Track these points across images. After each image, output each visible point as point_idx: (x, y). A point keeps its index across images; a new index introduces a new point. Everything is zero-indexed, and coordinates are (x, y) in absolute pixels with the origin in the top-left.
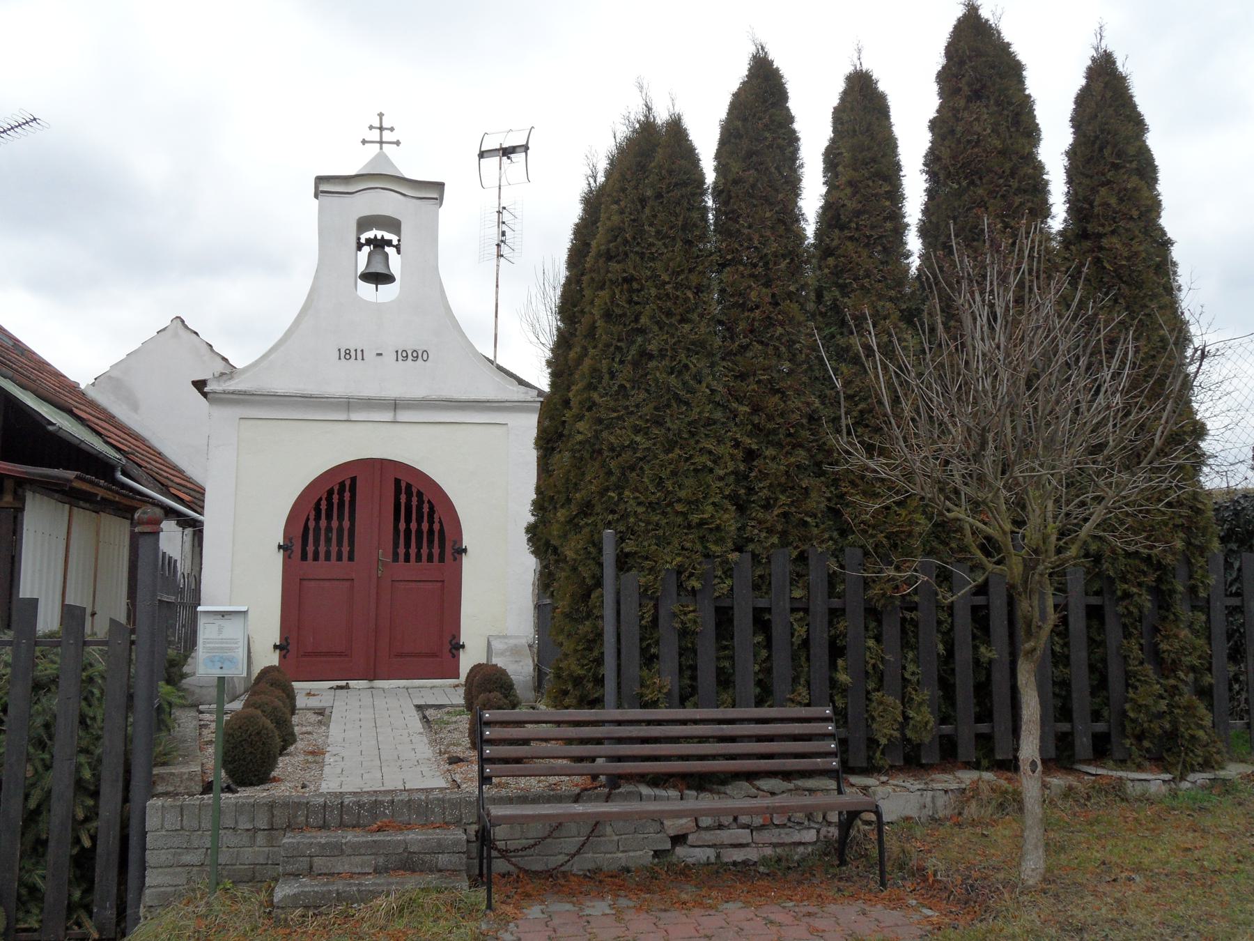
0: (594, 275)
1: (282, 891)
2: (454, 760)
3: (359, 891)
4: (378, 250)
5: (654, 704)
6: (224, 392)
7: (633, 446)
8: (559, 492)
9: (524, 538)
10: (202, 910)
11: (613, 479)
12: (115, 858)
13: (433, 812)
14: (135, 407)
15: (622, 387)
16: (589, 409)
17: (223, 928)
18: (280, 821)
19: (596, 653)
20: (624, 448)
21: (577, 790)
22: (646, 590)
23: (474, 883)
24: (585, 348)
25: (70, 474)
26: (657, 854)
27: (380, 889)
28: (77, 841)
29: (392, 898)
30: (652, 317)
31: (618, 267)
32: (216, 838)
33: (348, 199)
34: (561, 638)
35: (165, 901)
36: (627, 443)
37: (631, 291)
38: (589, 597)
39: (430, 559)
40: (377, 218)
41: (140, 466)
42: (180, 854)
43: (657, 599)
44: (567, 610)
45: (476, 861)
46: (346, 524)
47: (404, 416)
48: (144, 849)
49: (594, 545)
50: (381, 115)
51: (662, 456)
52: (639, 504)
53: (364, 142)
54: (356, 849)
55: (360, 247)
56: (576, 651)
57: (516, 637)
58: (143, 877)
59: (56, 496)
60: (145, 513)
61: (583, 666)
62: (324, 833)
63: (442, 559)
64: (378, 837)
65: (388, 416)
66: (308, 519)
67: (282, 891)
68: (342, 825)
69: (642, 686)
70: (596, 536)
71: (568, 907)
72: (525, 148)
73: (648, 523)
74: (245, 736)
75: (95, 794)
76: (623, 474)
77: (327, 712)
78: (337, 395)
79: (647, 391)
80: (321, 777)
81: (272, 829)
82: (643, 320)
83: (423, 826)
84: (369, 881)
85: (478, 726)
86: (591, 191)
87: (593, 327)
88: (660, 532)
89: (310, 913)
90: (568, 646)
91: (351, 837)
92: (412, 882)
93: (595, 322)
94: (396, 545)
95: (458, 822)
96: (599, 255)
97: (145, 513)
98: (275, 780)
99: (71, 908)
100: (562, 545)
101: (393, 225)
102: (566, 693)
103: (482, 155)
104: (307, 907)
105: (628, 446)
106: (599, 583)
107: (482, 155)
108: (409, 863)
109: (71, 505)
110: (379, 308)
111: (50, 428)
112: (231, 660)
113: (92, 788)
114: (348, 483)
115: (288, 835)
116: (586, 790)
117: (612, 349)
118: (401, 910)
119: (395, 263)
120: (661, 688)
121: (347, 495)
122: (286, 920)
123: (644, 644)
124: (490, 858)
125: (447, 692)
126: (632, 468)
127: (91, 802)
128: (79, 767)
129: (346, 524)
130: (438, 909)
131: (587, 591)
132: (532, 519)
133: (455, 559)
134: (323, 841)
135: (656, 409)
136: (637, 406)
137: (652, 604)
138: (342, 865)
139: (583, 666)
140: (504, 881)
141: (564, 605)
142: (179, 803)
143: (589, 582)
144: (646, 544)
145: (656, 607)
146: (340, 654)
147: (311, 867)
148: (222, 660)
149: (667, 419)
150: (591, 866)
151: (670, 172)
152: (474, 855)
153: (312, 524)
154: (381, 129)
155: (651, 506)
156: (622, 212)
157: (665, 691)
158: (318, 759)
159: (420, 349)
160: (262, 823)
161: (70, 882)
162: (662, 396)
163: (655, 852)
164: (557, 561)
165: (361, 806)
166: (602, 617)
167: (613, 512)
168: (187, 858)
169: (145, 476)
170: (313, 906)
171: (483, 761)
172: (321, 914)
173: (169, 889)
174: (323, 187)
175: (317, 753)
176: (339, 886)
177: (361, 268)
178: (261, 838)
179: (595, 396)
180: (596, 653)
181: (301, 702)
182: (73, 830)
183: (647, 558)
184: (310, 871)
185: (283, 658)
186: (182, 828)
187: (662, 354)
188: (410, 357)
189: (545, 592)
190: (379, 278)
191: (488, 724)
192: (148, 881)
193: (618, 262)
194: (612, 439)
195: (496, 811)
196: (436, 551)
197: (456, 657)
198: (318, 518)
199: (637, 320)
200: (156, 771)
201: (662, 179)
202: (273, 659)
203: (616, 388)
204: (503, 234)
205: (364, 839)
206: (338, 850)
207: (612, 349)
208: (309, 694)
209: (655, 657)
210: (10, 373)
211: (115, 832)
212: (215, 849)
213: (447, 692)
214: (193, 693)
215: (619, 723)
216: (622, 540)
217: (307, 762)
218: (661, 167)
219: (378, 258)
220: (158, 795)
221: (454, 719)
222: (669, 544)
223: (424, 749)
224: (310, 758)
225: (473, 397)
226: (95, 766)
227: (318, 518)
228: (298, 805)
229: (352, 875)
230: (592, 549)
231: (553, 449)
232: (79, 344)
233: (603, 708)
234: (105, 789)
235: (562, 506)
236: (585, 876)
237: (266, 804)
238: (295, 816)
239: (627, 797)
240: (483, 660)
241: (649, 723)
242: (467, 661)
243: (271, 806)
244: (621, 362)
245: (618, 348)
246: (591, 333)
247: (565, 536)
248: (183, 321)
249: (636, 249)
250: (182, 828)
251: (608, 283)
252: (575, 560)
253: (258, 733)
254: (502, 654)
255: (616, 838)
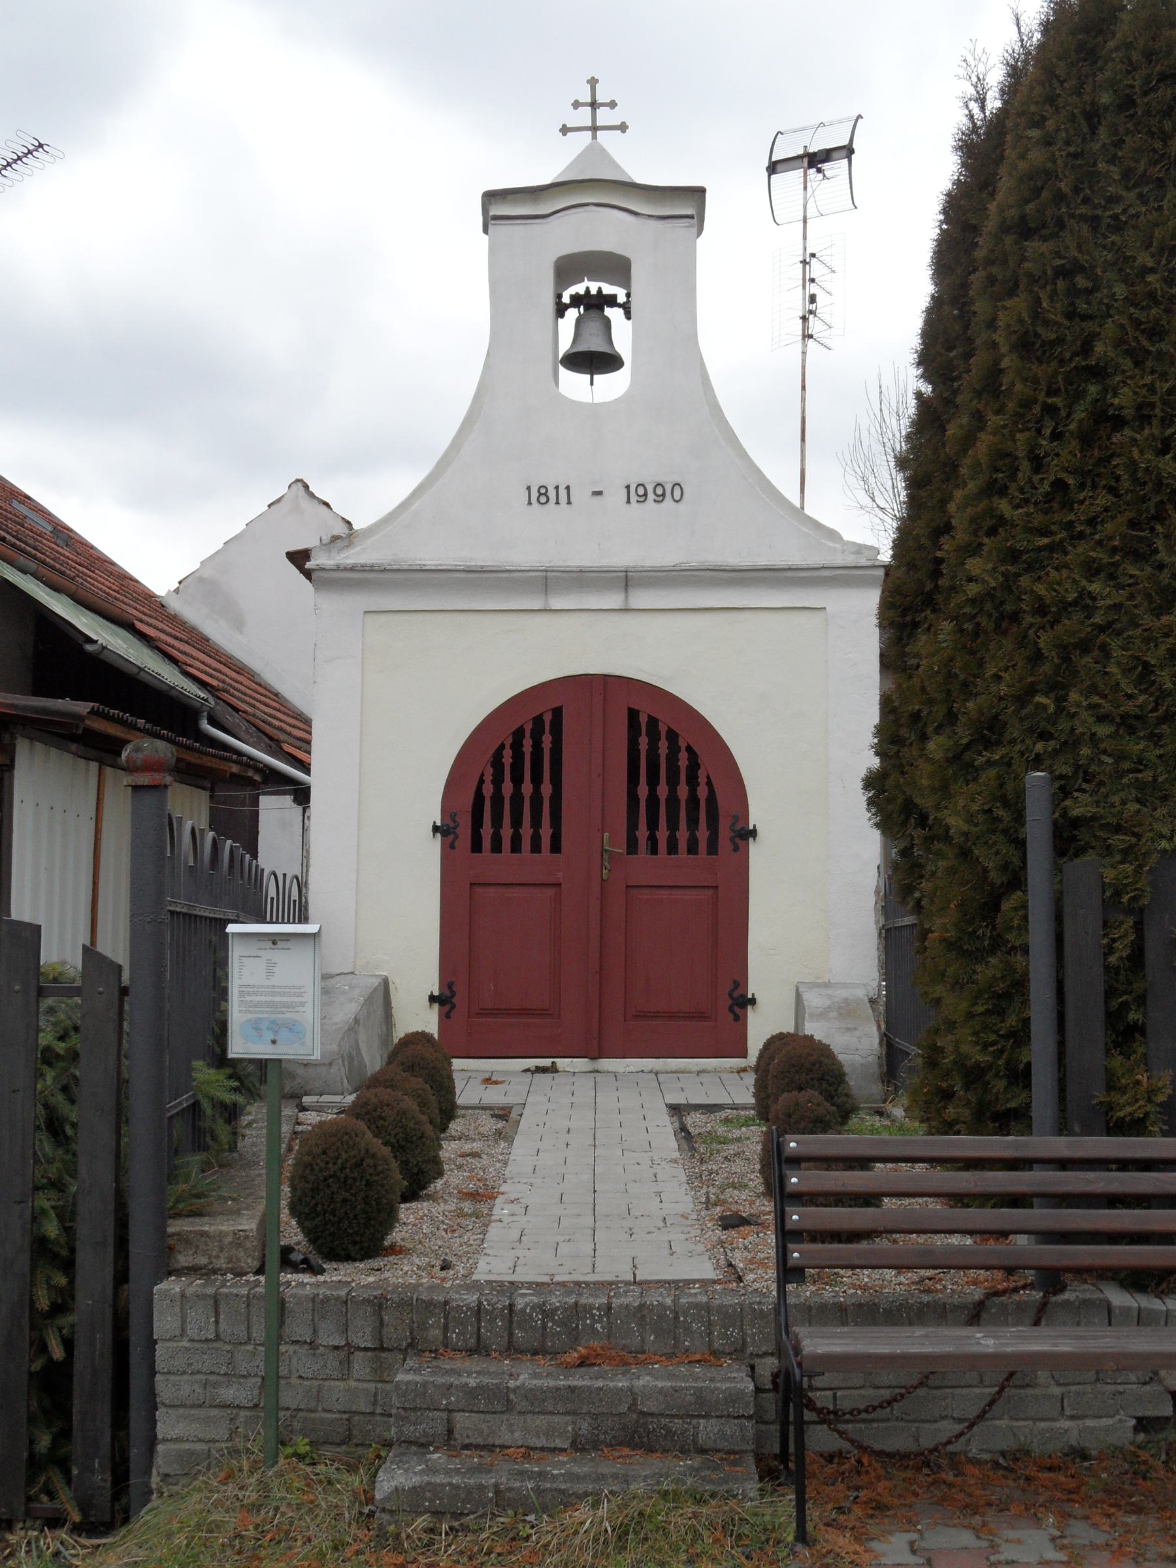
0: (994, 270)
1: (393, 1479)
2: (733, 1222)
3: (538, 1491)
4: (594, 313)
5: (1135, 1127)
6: (338, 569)
7: (1085, 603)
8: (931, 702)
9: (860, 798)
10: (251, 1495)
11: (1046, 668)
12: (105, 1384)
13: (688, 1329)
14: (239, 624)
15: (1059, 485)
16: (992, 532)
17: (285, 1536)
18: (396, 1332)
19: (1012, 1021)
20: (1065, 607)
21: (977, 1294)
22: (1117, 894)
23: (767, 1473)
24: (979, 418)
25: (82, 707)
26: (1143, 1424)
27: (580, 1488)
28: (43, 1348)
29: (604, 1510)
30: (1119, 342)
31: (1045, 247)
32: (273, 1357)
33: (537, 227)
34: (939, 990)
35: (191, 1465)
36: (1071, 596)
37: (1074, 292)
38: (997, 908)
39: (692, 849)
40: (589, 258)
41: (237, 710)
42: (216, 1385)
43: (1141, 910)
44: (951, 934)
45: (775, 1428)
46: (547, 789)
47: (642, 599)
48: (153, 1372)
49: (1006, 803)
50: (593, 82)
51: (1147, 620)
52: (1102, 719)
53: (565, 130)
54: (536, 1401)
55: (561, 310)
56: (970, 1015)
57: (845, 985)
58: (153, 1422)
59: (74, 747)
60: (138, 749)
61: (986, 1046)
62: (475, 1364)
63: (713, 848)
64: (580, 1380)
65: (614, 600)
66: (481, 781)
67: (393, 1479)
68: (512, 1350)
69: (1110, 1087)
70: (1009, 787)
71: (966, 1538)
72: (848, 151)
73: (1121, 757)
74: (333, 1168)
75: (68, 1266)
76: (1066, 659)
77: (514, 1115)
78: (527, 565)
79: (1113, 491)
80: (479, 1250)
81: (382, 1349)
82: (1099, 348)
83: (670, 1356)
84: (560, 1467)
85: (776, 1163)
86: (975, 129)
87: (995, 373)
88: (1147, 776)
89: (445, 1527)
90: (955, 1004)
91: (526, 1376)
92: (644, 1474)
93: (997, 362)
94: (632, 826)
95: (738, 1352)
96: (1004, 228)
97: (138, 749)
98: (394, 1250)
99: (35, 1464)
100: (937, 807)
101: (617, 267)
102: (948, 1096)
103: (773, 168)
104: (438, 1514)
105: (1075, 603)
106: (1016, 880)
107: (773, 168)
108: (639, 1433)
109: (102, 763)
110: (594, 411)
111: (89, 647)
112: (292, 1027)
113: (64, 1253)
114: (547, 718)
115: (410, 1363)
116: (996, 1294)
117: (1037, 409)
118: (622, 1534)
119: (623, 334)
120: (1151, 1093)
121: (547, 740)
122: (397, 1536)
123: (1115, 1004)
124: (801, 1425)
125: (726, 1083)
126: (1084, 647)
127: (61, 1280)
128: (37, 1217)
129: (547, 789)
130: (697, 1536)
131: (990, 904)
132: (875, 762)
133: (736, 849)
134: (472, 1382)
135: (1133, 524)
136: (1092, 522)
137: (1130, 921)
138: (511, 1431)
139: (986, 1046)
140: (830, 1469)
141: (942, 925)
142: (210, 1291)
143: (996, 877)
144: (1116, 799)
145: (1139, 927)
146: (543, 1013)
147: (450, 1432)
148: (275, 1026)
149: (1159, 543)
150: (1006, 1443)
151: (1149, 55)
152: (771, 1415)
153: (488, 790)
154: (594, 105)
155: (1128, 724)
156: (1048, 142)
157: (1161, 1098)
158: (483, 1208)
159: (668, 480)
160: (362, 1335)
161: (32, 1420)
162: (1144, 499)
163: (1139, 1420)
164: (928, 840)
165: (548, 1313)
166: (1025, 950)
167: (1044, 736)
168: (229, 1393)
169: (244, 725)
170: (451, 1512)
171: (786, 1235)
172: (465, 1528)
173: (199, 1447)
174: (496, 210)
175: (482, 1196)
176: (501, 1476)
177: (565, 344)
178: (361, 1365)
179: (1003, 506)
180: (1012, 1021)
181: (467, 1093)
182: (33, 1327)
183: (1118, 829)
184: (448, 1439)
185: (445, 1017)
186: (218, 1337)
187: (1143, 417)
188: (651, 496)
189: (903, 901)
190: (595, 361)
191: (796, 1161)
192: (161, 1430)
193: (1045, 239)
194: (1041, 589)
195: (817, 1343)
196: (703, 834)
197: (740, 1020)
198: (498, 781)
199: (1086, 349)
200: (174, 1227)
201: (1132, 68)
202: (428, 1021)
203: (1046, 487)
204: (813, 299)
205: (551, 1383)
206: (501, 1401)
207: (1037, 409)
208: (488, 1081)
209: (1138, 1029)
210: (33, 566)
211: (104, 1337)
212: (272, 1382)
213: (726, 1083)
214: (292, 1076)
215: (1064, 1164)
216: (1064, 792)
217: (461, 1214)
218: (1129, 46)
219: (593, 326)
220: (179, 1272)
221: (736, 1133)
222: (1164, 799)
223: (678, 1196)
224: (467, 1206)
225: (762, 562)
226: (67, 1216)
227: (498, 781)
228: (429, 1305)
229: (529, 1451)
230: (1000, 812)
231: (915, 625)
232: (152, 527)
233: (1028, 1130)
234: (85, 1258)
235: (938, 730)
236: (996, 1465)
237: (368, 1301)
238: (423, 1326)
239: (1081, 1312)
240: (789, 1028)
241: (1124, 1165)
242: (760, 1028)
243: (379, 1304)
244: (1056, 436)
245: (1051, 410)
246: (991, 385)
247: (944, 789)
248: (306, 487)
249: (1083, 210)
250: (218, 1337)
251: (1023, 282)
252: (966, 834)
253: (359, 1164)
254: (822, 1015)
255: (1057, 1391)
